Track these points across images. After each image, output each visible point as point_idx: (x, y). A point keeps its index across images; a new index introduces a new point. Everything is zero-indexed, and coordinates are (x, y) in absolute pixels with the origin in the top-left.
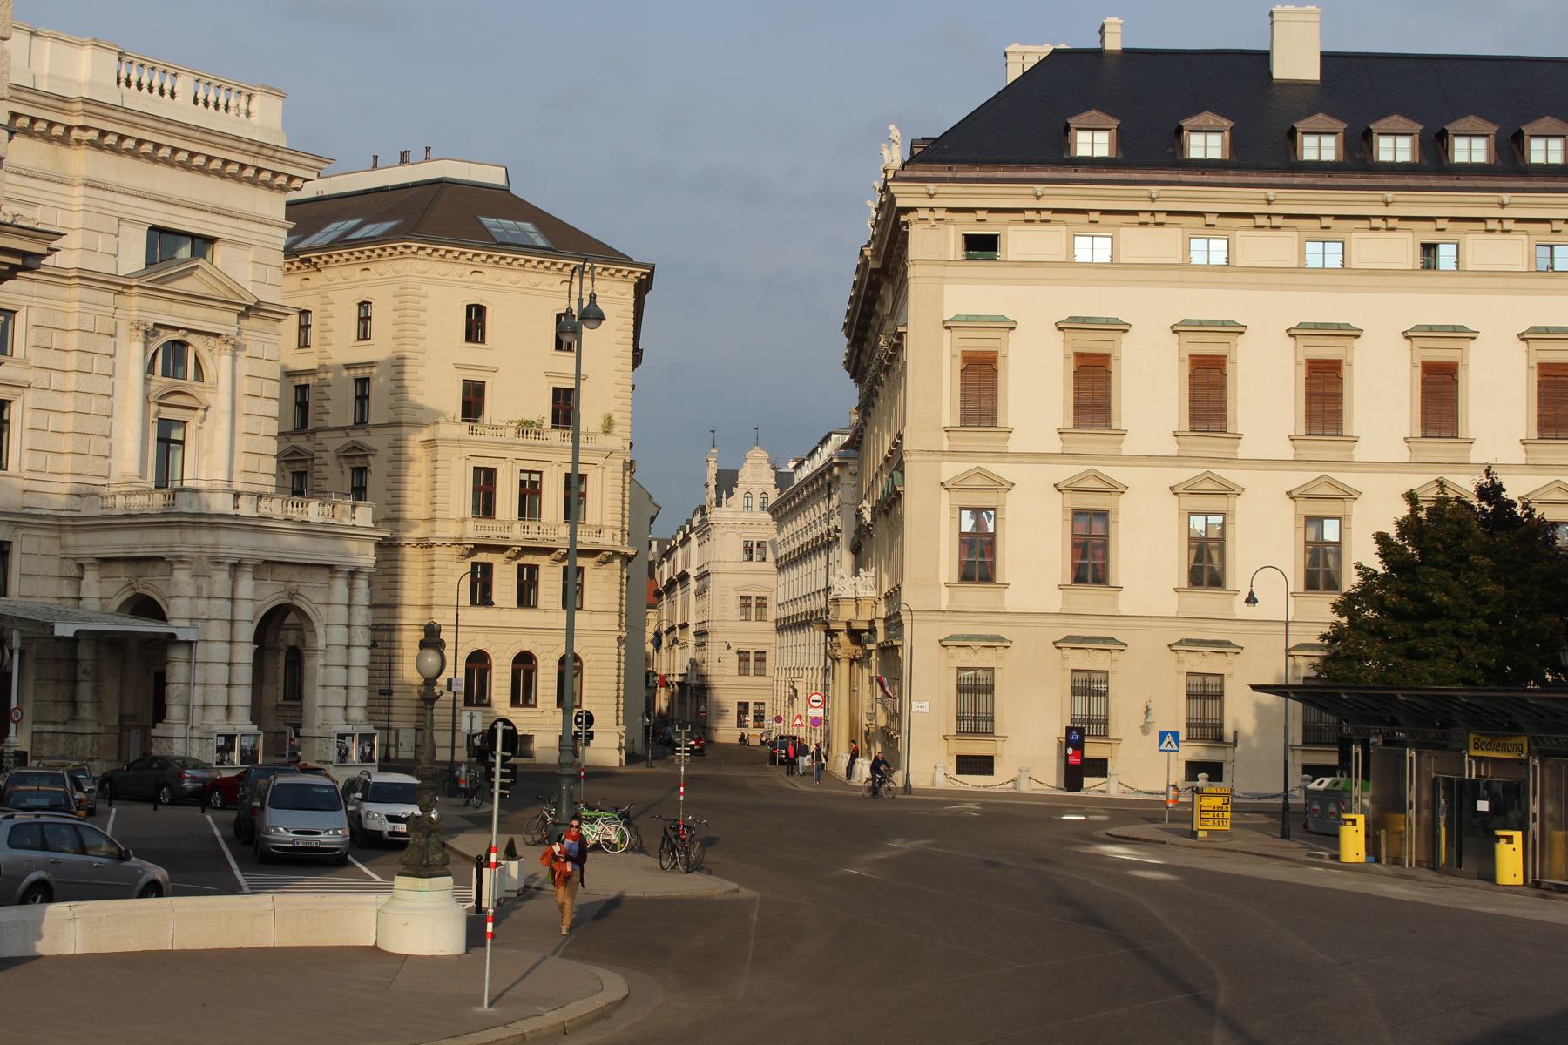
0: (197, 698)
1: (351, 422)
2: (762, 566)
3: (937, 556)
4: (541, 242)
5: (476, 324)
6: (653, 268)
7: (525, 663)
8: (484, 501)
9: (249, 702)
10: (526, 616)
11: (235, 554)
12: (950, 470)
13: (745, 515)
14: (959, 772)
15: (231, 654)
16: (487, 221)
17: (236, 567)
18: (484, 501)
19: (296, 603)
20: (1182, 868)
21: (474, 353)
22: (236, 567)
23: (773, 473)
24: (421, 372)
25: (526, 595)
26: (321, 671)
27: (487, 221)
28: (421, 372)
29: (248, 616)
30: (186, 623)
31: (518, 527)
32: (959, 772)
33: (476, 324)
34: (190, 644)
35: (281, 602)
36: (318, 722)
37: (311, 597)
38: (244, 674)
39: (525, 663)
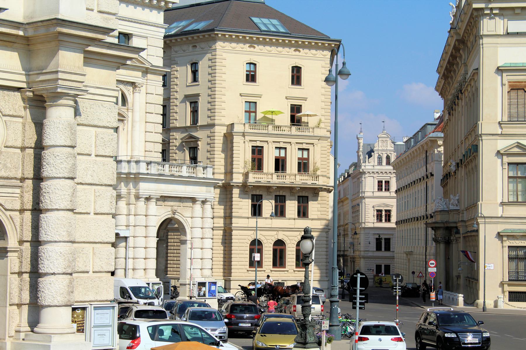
0: (130, 265)
1: (188, 124)
2: (387, 194)
3: (496, 188)
4: (282, 30)
5: (296, 75)
6: (340, 41)
7: (279, 245)
8: (258, 163)
9: (155, 268)
10: (278, 222)
11: (146, 194)
12: (502, 144)
13: (379, 167)
14: (510, 300)
15: (146, 242)
16: (256, 20)
17: (148, 199)
18: (258, 163)
19: (176, 216)
20: (364, 340)
21: (296, 91)
22: (148, 199)
23: (393, 146)
24: (224, 98)
25: (280, 212)
26: (189, 250)
27: (256, 20)
28: (224, 98)
29: (155, 223)
30: (125, 228)
31: (275, 176)
32: (510, 300)
33: (296, 75)
34: (126, 238)
35: (170, 216)
36: (188, 276)
37: (186, 215)
38: (153, 253)
39: (279, 245)
